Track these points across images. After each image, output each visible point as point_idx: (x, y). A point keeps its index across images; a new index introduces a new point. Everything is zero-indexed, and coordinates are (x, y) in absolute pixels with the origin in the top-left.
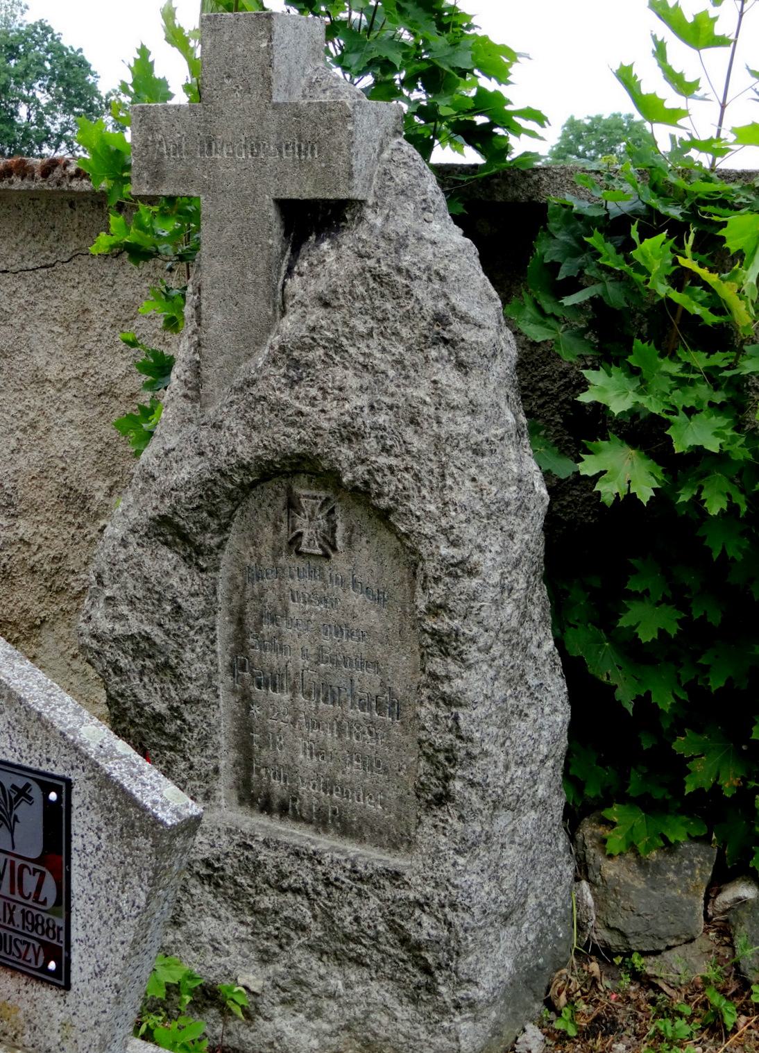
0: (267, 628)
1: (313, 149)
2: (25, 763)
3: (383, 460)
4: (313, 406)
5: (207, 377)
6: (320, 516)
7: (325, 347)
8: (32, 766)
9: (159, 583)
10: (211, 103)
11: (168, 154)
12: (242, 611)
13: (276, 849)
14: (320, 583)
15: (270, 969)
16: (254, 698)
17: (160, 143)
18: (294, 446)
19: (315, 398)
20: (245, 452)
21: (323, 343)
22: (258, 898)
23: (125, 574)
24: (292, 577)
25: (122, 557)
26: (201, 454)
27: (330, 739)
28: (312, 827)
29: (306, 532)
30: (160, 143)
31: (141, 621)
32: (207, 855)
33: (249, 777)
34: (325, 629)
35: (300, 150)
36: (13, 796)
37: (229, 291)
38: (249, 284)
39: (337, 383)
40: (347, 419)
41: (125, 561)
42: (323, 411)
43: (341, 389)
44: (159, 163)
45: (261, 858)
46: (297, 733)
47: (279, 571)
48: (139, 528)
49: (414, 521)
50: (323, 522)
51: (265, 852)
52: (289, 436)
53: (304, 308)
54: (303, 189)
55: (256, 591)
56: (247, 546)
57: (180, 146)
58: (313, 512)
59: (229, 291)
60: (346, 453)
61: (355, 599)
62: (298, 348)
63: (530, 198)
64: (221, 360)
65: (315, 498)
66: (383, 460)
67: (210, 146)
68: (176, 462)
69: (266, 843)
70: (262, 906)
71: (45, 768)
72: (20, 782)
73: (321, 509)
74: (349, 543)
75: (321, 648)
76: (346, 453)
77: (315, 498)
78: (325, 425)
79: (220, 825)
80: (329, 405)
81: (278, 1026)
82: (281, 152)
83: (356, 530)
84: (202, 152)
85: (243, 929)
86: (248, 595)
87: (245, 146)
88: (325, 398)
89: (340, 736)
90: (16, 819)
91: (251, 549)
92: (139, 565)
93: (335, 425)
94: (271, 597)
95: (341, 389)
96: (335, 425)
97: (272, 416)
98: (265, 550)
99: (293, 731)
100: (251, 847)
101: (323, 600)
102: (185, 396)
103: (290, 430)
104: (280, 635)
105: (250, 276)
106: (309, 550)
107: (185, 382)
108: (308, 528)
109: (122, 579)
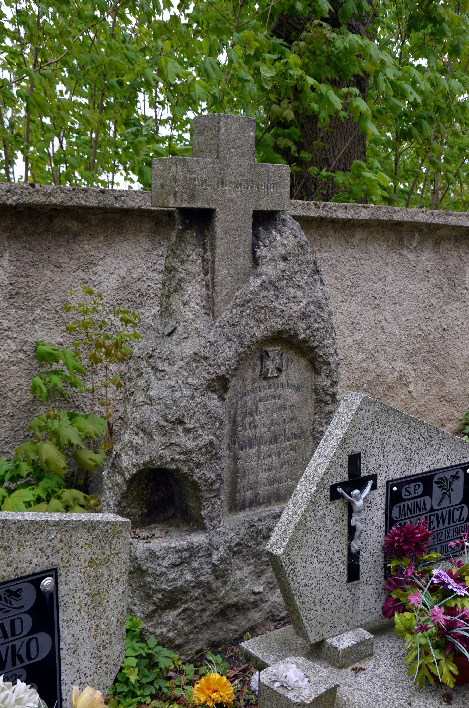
0: (248, 420)
1: (273, 187)
2: (454, 464)
3: (316, 326)
4: (286, 307)
5: (218, 302)
6: (277, 358)
7: (287, 279)
8: (457, 464)
9: (215, 412)
10: (224, 160)
11: (199, 186)
12: (235, 415)
13: (265, 520)
14: (273, 390)
15: (263, 579)
16: (239, 456)
17: (194, 179)
18: (279, 327)
19: (286, 303)
20: (258, 334)
21: (286, 277)
22: (258, 548)
23: (197, 413)
24: (260, 391)
25: (193, 405)
26: (230, 340)
27: (275, 460)
28: (264, 505)
29: (271, 367)
30: (194, 179)
31: (208, 435)
32: (238, 540)
33: (235, 496)
34: (274, 410)
35: (268, 187)
36: (451, 480)
37: (230, 257)
38: (241, 253)
39: (293, 295)
40: (303, 310)
41: (196, 406)
42: (291, 308)
43: (294, 298)
44: (193, 190)
45: (260, 528)
46: (259, 464)
47: (254, 390)
48: (200, 387)
49: (326, 349)
50: (278, 361)
51: (261, 524)
52: (277, 323)
53: (275, 262)
54: (265, 207)
55: (243, 403)
56: (239, 382)
57: (206, 181)
58: (274, 357)
59: (230, 257)
60: (302, 325)
61: (288, 392)
62: (278, 281)
63: (139, 207)
64: (225, 292)
65: (275, 350)
66: (316, 326)
67: (222, 183)
68: (220, 347)
69: (260, 520)
70: (261, 550)
71: (462, 461)
72: (453, 473)
73: (277, 355)
74: (287, 368)
75: (272, 420)
76: (302, 325)
77: (275, 350)
78: (294, 314)
79: (237, 523)
80: (292, 305)
81: (273, 600)
82: (258, 188)
83: (290, 361)
84: (218, 186)
85: (250, 567)
86: (239, 406)
87: (241, 184)
88: (289, 303)
89: (279, 457)
90: (452, 490)
91: (241, 383)
92: (205, 406)
93: (298, 314)
94: (250, 403)
95: (294, 298)
96: (298, 314)
97: (270, 314)
98: (249, 381)
99: (257, 465)
100: (254, 526)
101: (274, 397)
102: (206, 313)
103: (278, 320)
104: (254, 420)
105: (241, 248)
106: (272, 376)
107: (204, 307)
108: (270, 365)
109: (197, 417)
